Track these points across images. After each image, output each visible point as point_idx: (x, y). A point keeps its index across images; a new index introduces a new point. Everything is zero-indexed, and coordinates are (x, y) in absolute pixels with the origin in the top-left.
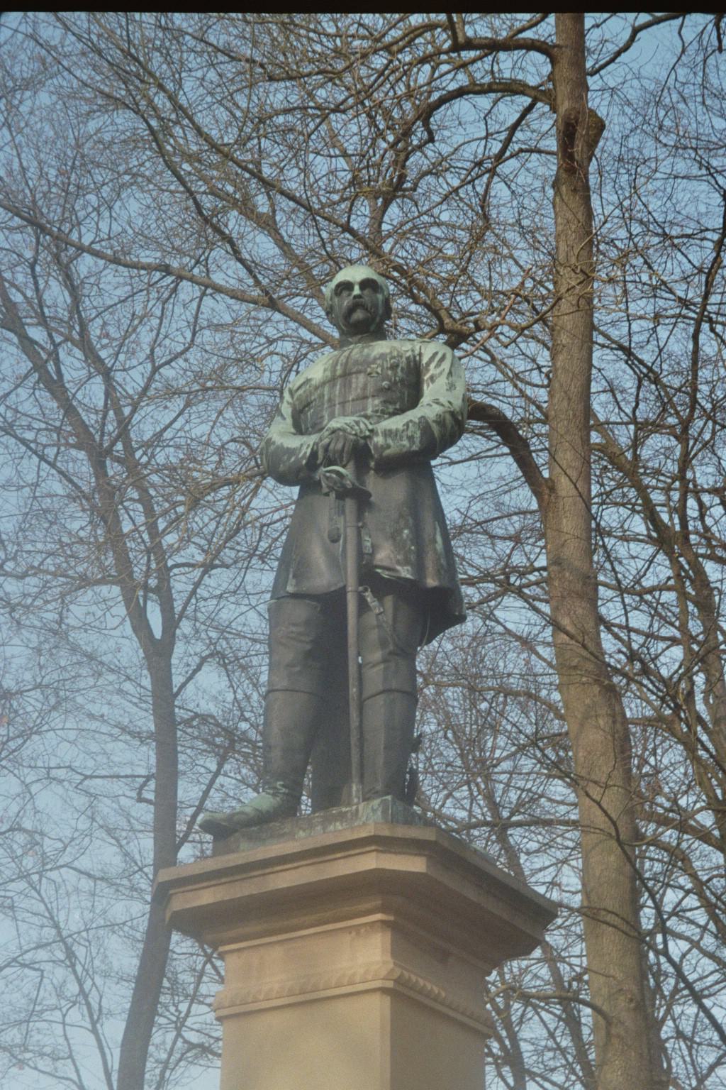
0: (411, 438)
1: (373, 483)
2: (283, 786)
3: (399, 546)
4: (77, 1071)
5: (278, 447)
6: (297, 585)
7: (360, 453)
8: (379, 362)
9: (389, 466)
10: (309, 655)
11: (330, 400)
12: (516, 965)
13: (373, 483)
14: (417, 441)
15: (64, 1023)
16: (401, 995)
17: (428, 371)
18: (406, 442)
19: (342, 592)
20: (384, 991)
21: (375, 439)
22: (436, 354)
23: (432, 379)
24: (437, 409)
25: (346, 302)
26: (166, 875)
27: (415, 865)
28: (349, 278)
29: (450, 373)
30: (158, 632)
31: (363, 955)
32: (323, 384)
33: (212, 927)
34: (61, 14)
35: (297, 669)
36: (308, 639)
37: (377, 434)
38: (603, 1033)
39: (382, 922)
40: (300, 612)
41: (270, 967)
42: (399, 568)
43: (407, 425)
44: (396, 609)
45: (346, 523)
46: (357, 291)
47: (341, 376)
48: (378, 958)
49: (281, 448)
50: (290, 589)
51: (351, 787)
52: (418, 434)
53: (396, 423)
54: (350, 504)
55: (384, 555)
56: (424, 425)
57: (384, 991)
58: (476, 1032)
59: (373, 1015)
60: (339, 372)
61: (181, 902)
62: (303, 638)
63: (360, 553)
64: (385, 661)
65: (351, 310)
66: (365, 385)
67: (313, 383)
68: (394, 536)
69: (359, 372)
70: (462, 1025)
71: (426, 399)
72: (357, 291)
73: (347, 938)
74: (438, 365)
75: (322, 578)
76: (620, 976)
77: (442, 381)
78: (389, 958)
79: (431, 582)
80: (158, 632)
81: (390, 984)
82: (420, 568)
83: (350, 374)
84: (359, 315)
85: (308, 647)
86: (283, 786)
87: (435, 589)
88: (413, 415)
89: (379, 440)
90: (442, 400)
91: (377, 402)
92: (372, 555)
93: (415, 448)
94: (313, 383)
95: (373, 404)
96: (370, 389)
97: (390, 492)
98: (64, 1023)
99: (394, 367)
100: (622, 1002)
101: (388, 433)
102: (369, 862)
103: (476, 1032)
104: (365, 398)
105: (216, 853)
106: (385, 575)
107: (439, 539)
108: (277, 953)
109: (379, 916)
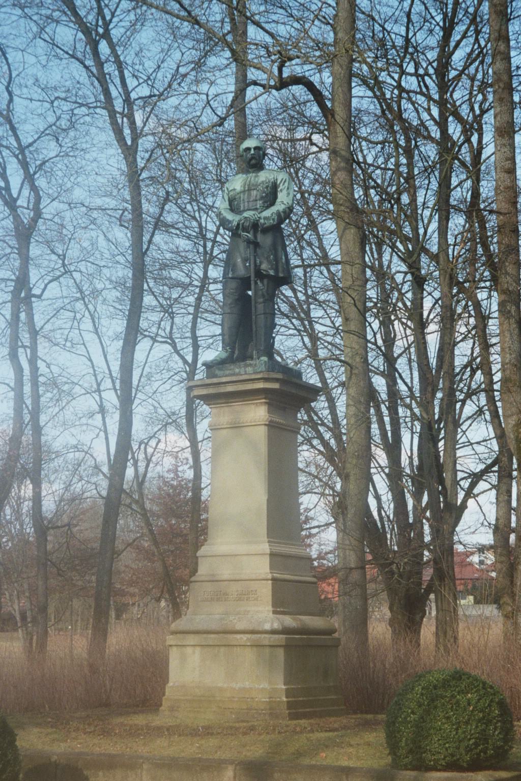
0: (273, 220)
1: (260, 237)
3: (269, 262)
4: (88, 352)
6: (233, 273)
7: (255, 226)
9: (266, 230)
10: (237, 300)
12: (316, 84)
13: (260, 237)
15: (79, 329)
16: (271, 425)
18: (272, 221)
19: (250, 277)
20: (265, 425)
23: (281, 190)
24: (283, 207)
25: (249, 156)
26: (191, 384)
27: (276, 386)
28: (249, 146)
29: (288, 188)
30: (129, 143)
31: (257, 413)
32: (241, 192)
33: (208, 399)
38: (349, 372)
40: (233, 285)
41: (226, 414)
43: (272, 214)
44: (268, 283)
45: (249, 252)
46: (252, 152)
50: (230, 276)
53: (267, 213)
54: (251, 246)
55: (264, 266)
56: (278, 213)
57: (265, 425)
58: (295, 432)
59: (260, 434)
61: (197, 392)
63: (255, 265)
64: (264, 302)
65: (251, 160)
68: (268, 258)
70: (289, 430)
71: (279, 200)
72: (252, 152)
73: (253, 406)
75: (241, 272)
76: (357, 347)
77: (285, 192)
78: (267, 414)
79: (281, 275)
80: (129, 143)
81: (267, 423)
82: (277, 270)
84: (253, 162)
85: (237, 297)
87: (282, 278)
88: (274, 209)
89: (262, 221)
90: (285, 202)
92: (260, 266)
95: (259, 203)
96: (258, 197)
97: (266, 241)
98: (79, 329)
99: (267, 187)
100: (358, 359)
101: (265, 218)
102: (261, 385)
103: (295, 432)
104: (256, 200)
105: (207, 377)
106: (264, 273)
107: (284, 257)
108: (226, 409)
109: (264, 400)
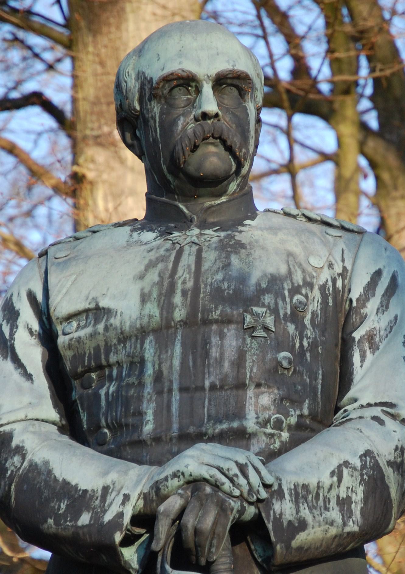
0: (344, 504)
5: (33, 466)
11: (158, 377)
14: (357, 509)
17: (364, 318)
18: (335, 514)
21: (277, 506)
22: (378, 274)
32: (142, 333)
37: (280, 494)
39: (231, 170)
47: (185, 323)
48: (238, 548)
49: (39, 475)
51: (35, 22)
52: (358, 496)
60: (179, 314)
66: (241, 355)
67: (115, 321)
69: (226, 321)
74: (384, 307)
83: (207, 322)
91: (266, 399)
93: (352, 527)
94: (115, 321)
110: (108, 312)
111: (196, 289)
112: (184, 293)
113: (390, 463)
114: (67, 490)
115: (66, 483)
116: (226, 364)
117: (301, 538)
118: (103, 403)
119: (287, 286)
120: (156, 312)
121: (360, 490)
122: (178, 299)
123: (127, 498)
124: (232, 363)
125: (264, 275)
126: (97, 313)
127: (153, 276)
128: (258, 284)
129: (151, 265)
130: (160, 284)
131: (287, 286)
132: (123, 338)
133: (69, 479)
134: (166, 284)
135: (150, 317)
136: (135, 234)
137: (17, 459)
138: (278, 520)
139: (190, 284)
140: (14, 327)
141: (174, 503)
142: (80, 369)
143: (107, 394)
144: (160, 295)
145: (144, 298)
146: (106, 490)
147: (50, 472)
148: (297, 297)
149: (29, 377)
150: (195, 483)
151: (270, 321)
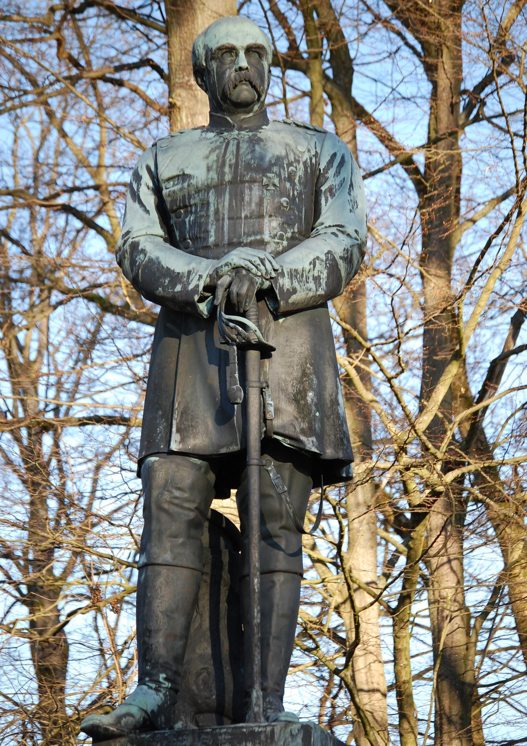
0: (317, 279)
2: (165, 679)
5: (151, 260)
8: (275, 169)
11: (217, 212)
14: (323, 282)
17: (327, 179)
18: (312, 285)
21: (281, 281)
22: (335, 155)
34: (135, 640)
35: (181, 540)
36: (192, 506)
37: (282, 274)
42: (303, 438)
47: (231, 182)
52: (324, 275)
62: (186, 505)
83: (243, 182)
85: (192, 515)
86: (165, 679)
106: (286, 443)
110: (189, 176)
111: (237, 164)
112: (230, 166)
113: (341, 258)
114: (169, 272)
115: (168, 269)
116: (253, 205)
117: (293, 298)
118: (188, 226)
119: (286, 162)
120: (215, 176)
121: (325, 272)
122: (227, 169)
123: (201, 277)
124: (256, 204)
125: (273, 156)
126: (184, 177)
127: (213, 157)
128: (270, 161)
129: (213, 150)
130: (217, 161)
131: (286, 162)
132: (198, 191)
133: (169, 267)
134: (220, 161)
135: (212, 179)
136: (204, 134)
137: (142, 256)
138: (281, 289)
139: (233, 161)
140: (139, 185)
141: (225, 280)
142: (175, 208)
143: (189, 221)
144: (217, 167)
145: (209, 169)
146: (189, 272)
147: (159, 263)
148: (291, 168)
149: (148, 212)
150: (237, 269)
151: (276, 181)
